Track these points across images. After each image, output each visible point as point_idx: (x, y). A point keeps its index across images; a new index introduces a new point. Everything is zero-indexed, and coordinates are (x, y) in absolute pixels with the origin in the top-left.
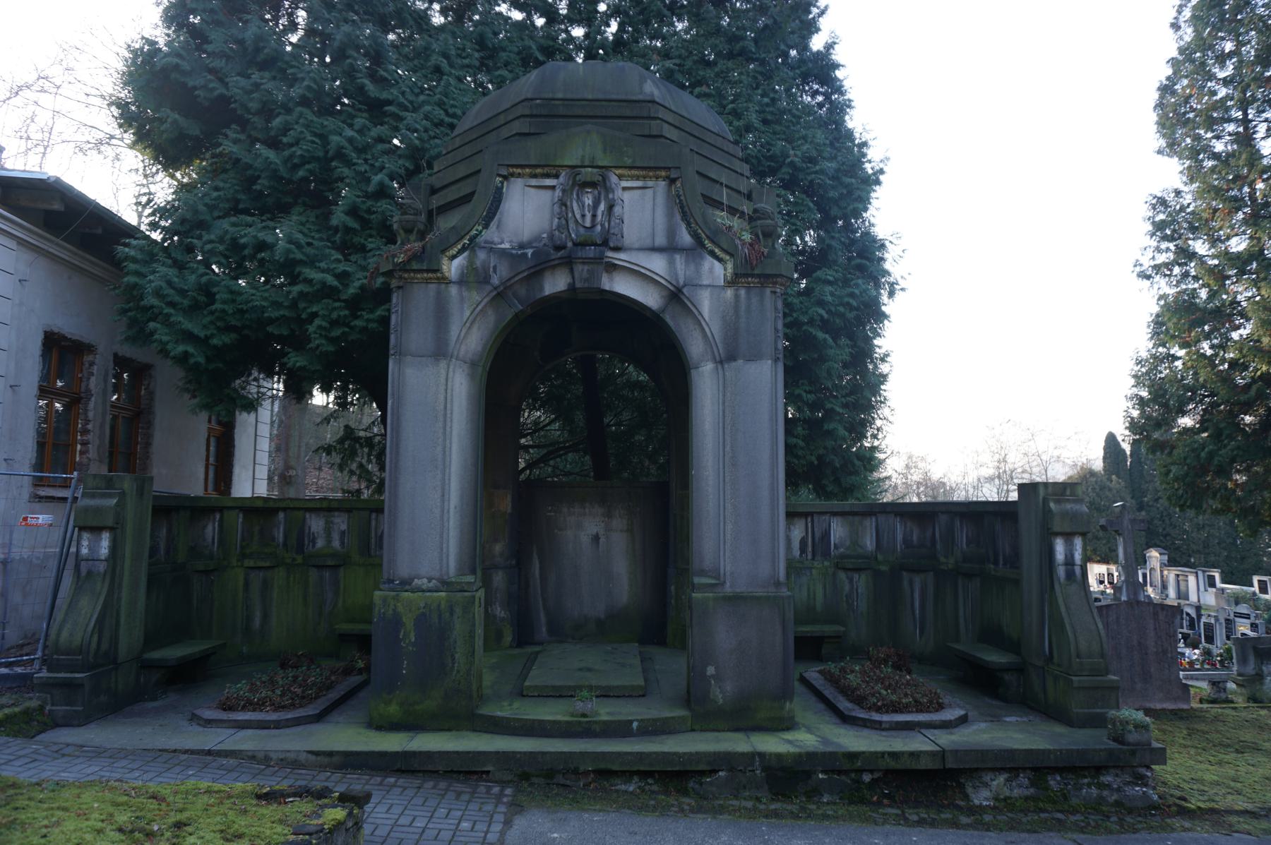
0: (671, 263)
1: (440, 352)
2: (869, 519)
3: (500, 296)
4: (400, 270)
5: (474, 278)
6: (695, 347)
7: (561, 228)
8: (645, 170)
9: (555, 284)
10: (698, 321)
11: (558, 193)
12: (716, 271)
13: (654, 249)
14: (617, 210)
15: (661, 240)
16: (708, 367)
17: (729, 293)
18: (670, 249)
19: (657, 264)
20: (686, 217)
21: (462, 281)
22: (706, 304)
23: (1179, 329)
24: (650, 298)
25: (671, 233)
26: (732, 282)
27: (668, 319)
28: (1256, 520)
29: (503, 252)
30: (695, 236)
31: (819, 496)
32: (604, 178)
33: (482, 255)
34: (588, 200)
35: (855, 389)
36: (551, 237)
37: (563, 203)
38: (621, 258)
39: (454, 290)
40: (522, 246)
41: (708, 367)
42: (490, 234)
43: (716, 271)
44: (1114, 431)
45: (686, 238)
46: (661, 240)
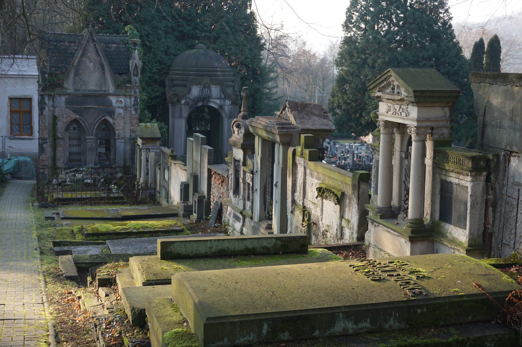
0: (220, 101)
1: (181, 117)
2: (117, 143)
3: (191, 107)
4: (18, 24)
5: (186, 104)
6: (224, 115)
7: (202, 95)
8: (216, 84)
9: (200, 104)
10: (225, 111)
11: (201, 89)
12: (228, 102)
13: (217, 98)
14: (211, 92)
15: (219, 97)
16: (226, 119)
17: (230, 107)
18: (220, 98)
19: (218, 101)
20: (223, 93)
21: (185, 104)
22: (226, 108)
23: (405, 37)
24: (216, 107)
25: (221, 95)
26: (231, 105)
27: (219, 110)
28: (3, 155)
29: (191, 99)
30: (225, 96)
31: (354, 186)
32: (210, 86)
33: (188, 100)
34: (207, 90)
35: (254, 28)
36: (200, 96)
37: (202, 91)
38: (212, 100)
39: (183, 106)
40: (195, 98)
41: (226, 119)
42: (189, 96)
43: (228, 102)
44: (500, 36)
45: (223, 96)
46: (219, 97)
